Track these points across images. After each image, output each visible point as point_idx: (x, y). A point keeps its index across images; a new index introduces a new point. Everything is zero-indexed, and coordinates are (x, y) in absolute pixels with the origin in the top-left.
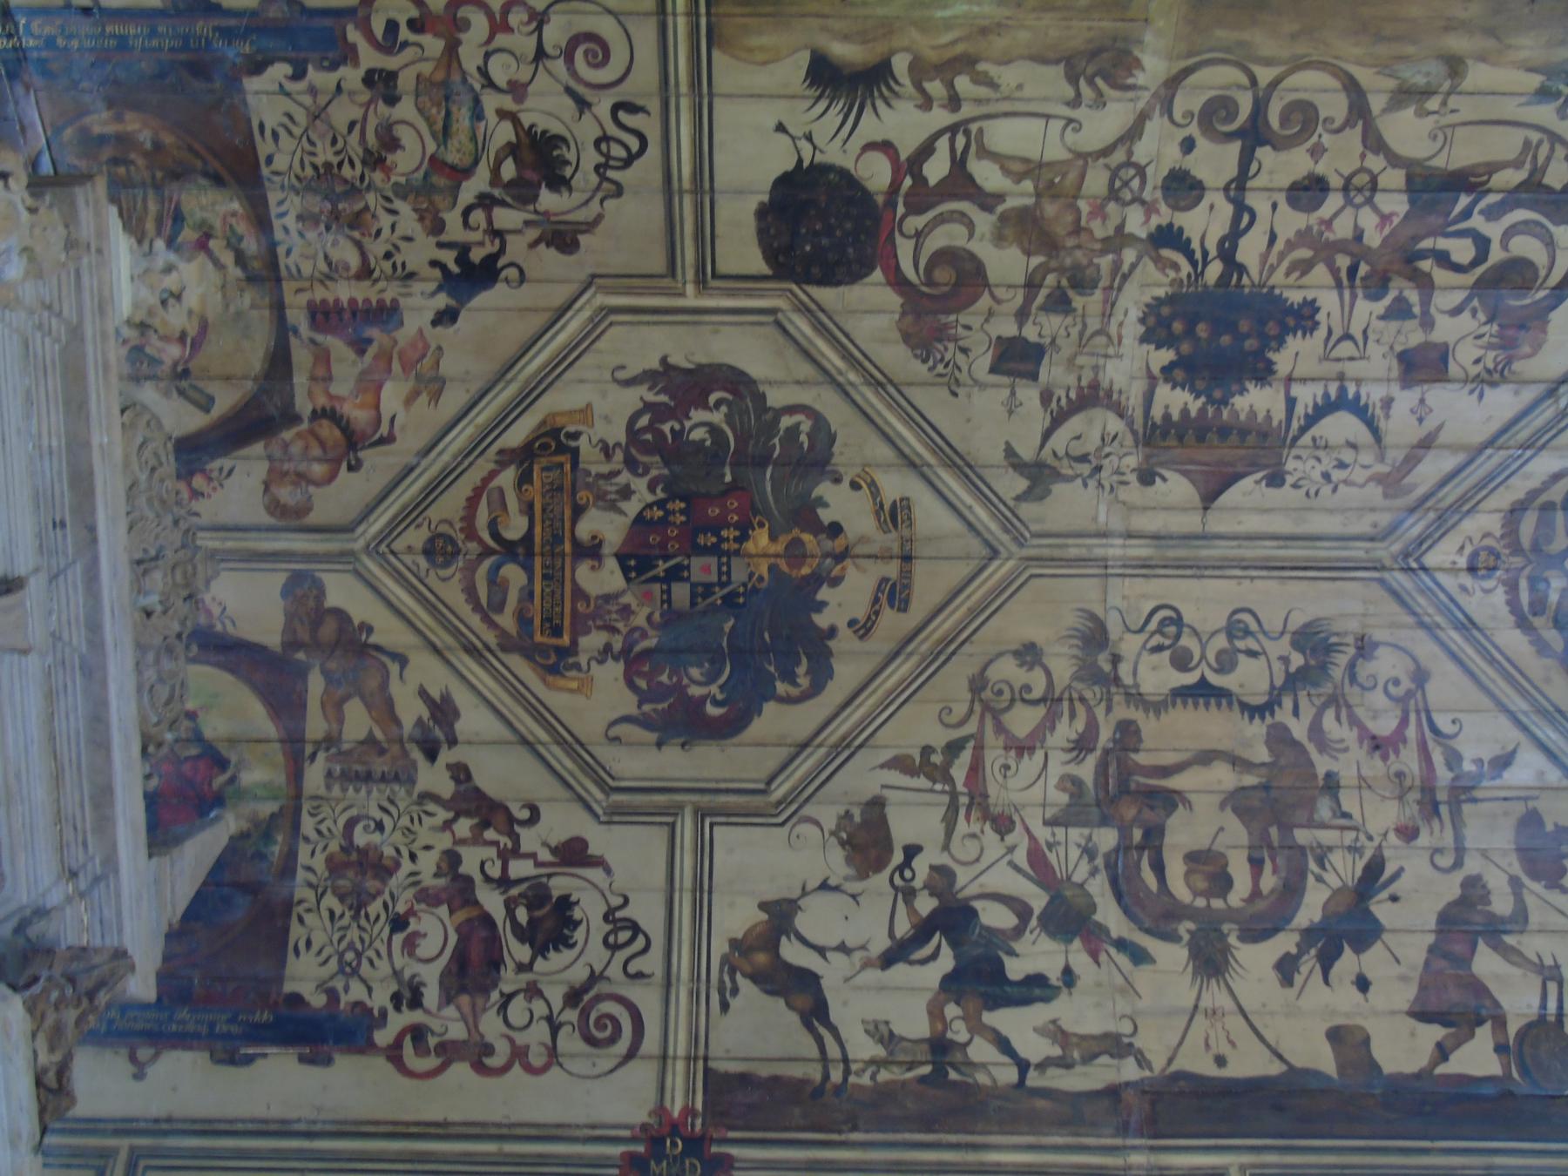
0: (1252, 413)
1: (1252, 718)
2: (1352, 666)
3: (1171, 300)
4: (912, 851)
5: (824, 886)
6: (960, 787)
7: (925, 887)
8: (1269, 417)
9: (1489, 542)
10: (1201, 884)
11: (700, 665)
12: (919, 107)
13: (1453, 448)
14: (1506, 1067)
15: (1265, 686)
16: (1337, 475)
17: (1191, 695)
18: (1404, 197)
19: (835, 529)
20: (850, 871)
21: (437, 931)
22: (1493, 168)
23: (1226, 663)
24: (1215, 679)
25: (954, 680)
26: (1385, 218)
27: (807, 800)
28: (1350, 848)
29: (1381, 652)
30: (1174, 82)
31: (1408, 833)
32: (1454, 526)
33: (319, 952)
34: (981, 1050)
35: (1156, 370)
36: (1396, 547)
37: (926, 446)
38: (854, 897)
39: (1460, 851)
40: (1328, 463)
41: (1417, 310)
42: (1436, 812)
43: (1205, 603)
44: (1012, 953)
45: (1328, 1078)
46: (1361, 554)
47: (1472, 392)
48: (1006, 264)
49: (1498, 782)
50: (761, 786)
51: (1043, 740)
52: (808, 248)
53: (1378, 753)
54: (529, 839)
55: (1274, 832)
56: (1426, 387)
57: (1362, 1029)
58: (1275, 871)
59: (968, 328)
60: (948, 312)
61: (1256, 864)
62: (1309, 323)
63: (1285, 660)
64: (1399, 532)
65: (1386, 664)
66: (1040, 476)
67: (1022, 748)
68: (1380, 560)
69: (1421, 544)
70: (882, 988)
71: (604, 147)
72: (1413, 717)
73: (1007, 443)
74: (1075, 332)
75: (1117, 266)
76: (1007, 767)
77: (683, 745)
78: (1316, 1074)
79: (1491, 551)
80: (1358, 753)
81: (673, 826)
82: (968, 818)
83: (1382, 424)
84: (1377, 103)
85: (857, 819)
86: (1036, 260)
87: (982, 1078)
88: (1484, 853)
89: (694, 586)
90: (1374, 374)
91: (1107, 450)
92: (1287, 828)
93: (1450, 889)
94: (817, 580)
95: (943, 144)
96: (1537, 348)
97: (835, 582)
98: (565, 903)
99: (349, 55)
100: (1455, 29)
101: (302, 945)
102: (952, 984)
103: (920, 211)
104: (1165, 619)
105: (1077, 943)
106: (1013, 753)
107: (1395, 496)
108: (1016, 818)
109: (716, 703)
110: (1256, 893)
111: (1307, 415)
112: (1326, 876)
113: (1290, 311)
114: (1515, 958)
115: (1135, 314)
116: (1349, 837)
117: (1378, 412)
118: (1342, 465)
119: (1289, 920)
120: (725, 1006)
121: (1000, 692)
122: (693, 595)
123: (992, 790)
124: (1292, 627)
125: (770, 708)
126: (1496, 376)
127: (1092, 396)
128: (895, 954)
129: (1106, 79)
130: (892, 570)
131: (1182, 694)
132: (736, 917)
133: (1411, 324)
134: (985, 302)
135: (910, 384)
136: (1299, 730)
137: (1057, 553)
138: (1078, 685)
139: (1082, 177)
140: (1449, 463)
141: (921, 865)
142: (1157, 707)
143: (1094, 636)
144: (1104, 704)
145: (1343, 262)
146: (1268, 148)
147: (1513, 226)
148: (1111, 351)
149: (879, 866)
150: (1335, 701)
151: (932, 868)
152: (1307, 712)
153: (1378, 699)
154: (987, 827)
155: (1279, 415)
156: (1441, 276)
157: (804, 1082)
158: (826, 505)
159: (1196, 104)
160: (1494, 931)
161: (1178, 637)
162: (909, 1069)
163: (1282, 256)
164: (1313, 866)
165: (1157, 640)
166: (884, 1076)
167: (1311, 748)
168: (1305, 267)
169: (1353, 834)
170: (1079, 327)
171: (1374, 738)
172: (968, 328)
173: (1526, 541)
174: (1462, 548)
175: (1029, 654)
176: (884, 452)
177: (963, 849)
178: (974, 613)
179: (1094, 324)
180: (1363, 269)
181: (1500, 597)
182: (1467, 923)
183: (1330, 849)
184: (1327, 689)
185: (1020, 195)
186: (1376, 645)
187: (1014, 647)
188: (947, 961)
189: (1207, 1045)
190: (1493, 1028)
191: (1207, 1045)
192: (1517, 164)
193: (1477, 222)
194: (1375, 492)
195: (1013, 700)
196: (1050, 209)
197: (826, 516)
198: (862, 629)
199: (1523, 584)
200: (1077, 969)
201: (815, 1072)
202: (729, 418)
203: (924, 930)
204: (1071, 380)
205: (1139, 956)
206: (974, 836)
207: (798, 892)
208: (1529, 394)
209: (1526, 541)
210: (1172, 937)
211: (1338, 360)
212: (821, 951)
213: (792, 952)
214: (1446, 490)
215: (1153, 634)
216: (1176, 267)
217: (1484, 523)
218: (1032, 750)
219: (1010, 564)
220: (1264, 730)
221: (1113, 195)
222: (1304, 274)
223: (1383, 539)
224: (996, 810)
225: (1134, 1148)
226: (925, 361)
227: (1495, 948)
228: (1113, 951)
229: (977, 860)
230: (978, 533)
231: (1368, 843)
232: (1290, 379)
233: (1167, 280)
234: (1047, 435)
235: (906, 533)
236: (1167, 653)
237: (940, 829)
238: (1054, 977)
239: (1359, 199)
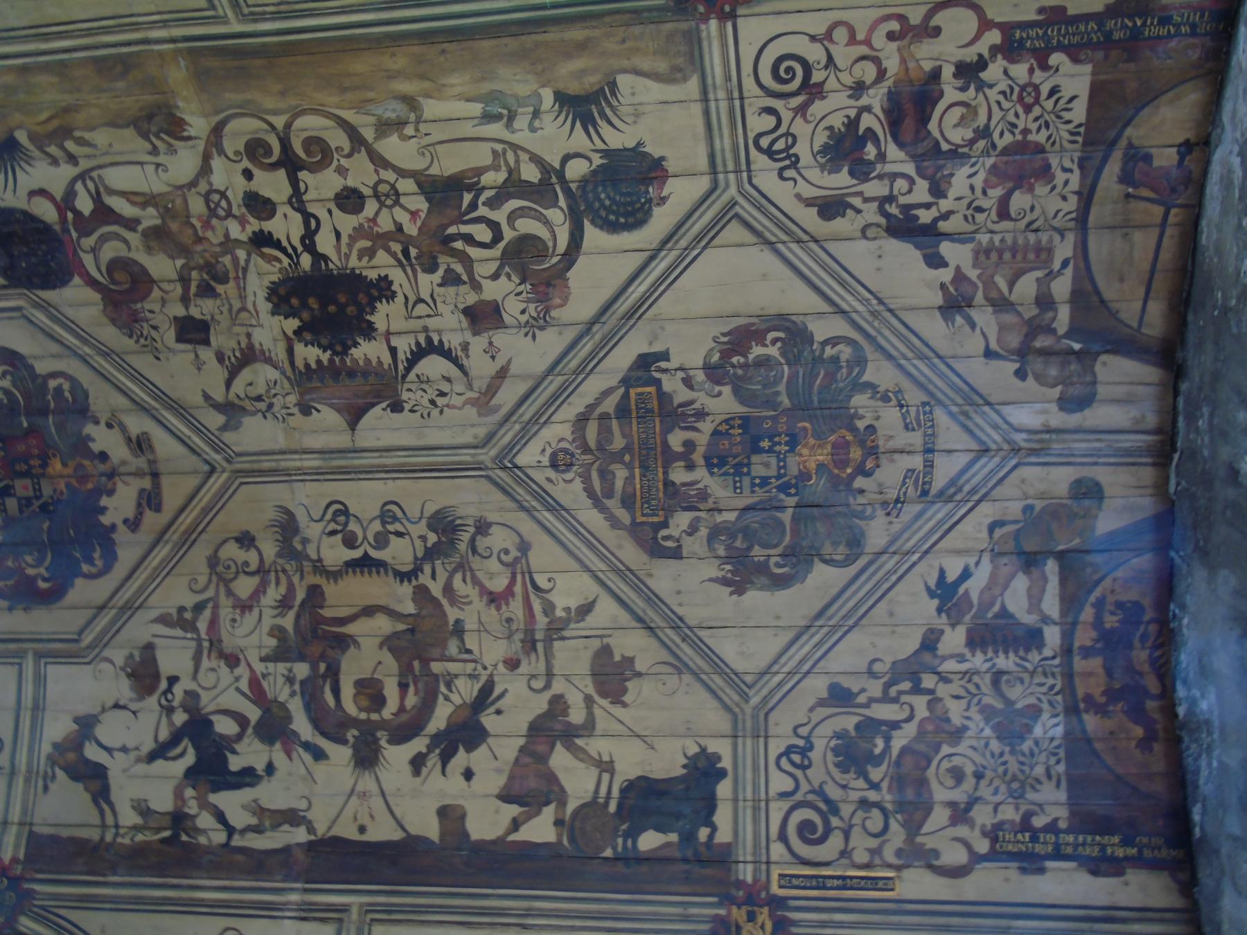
0: (368, 361)
1: (402, 581)
2: (473, 541)
3: (282, 282)
4: (173, 680)
5: (117, 706)
6: (203, 636)
7: (181, 706)
8: (380, 363)
9: (564, 445)
10: (365, 703)
11: (31, 554)
12: (50, 164)
13: (522, 377)
14: (559, 836)
15: (410, 558)
16: (440, 401)
17: (359, 566)
18: (422, 198)
19: (103, 456)
20: (133, 695)
22: (479, 171)
23: (381, 541)
24: (374, 554)
25: (198, 557)
26: (414, 214)
27: (105, 646)
28: (470, 676)
29: (494, 529)
30: (217, 130)
31: (512, 664)
32: (536, 433)
34: (205, 820)
35: (290, 334)
36: (493, 453)
37: (149, 395)
38: (134, 713)
39: (550, 675)
40: (432, 393)
41: (465, 277)
42: (534, 649)
43: (365, 498)
44: (234, 752)
45: (433, 842)
46: (468, 458)
47: (526, 335)
48: (161, 266)
49: (582, 625)
50: (75, 637)
51: (258, 602)
52: (24, 265)
53: (493, 605)
54: (871, 214)
55: (416, 664)
56: (491, 333)
57: (462, 807)
58: (416, 693)
59: (151, 312)
60: (136, 302)
61: (403, 687)
62: (389, 293)
63: (423, 538)
64: (493, 441)
65: (498, 539)
66: (232, 411)
67: (244, 607)
68: (482, 463)
69: (511, 449)
70: (147, 776)
72: (519, 578)
73: (203, 391)
74: (225, 309)
75: (235, 260)
76: (234, 620)
77: (25, 610)
78: (425, 840)
79: (565, 451)
80: (478, 604)
81: (20, 665)
82: (209, 657)
83: (465, 362)
84: (368, 134)
85: (137, 659)
86: (180, 262)
87: (202, 840)
88: (567, 678)
89: (19, 499)
90: (449, 325)
91: (273, 392)
92: (425, 662)
93: (540, 704)
94: (99, 492)
95: (79, 186)
96: (565, 300)
97: (111, 493)
100: (395, 77)
102: (192, 774)
103: (88, 234)
104: (336, 511)
105: (278, 746)
106: (238, 611)
107: (486, 415)
108: (241, 657)
109: (45, 580)
110: (402, 709)
111: (407, 359)
112: (452, 696)
113: (371, 284)
114: (582, 756)
115: (262, 294)
116: (470, 667)
117: (460, 353)
118: (442, 394)
119: (422, 729)
120: (46, 788)
121: (229, 567)
122: (20, 505)
123: (225, 636)
124: (427, 513)
125: (79, 582)
126: (542, 322)
127: (249, 356)
128: (160, 752)
129: (169, 134)
130: (147, 483)
131: (353, 565)
132: (57, 728)
133: (464, 289)
134: (156, 293)
135: (127, 353)
136: (436, 589)
137: (256, 466)
138: (280, 561)
139: (186, 202)
140: (522, 388)
141: (178, 690)
142: (334, 575)
143: (287, 526)
144: (298, 574)
145: (397, 247)
146: (305, 172)
147: (513, 212)
148: (254, 322)
149: (150, 690)
150: (461, 567)
151: (186, 692)
152: (442, 576)
153: (493, 564)
154: (222, 663)
155: (387, 359)
156: (474, 252)
157: (87, 841)
158: (93, 440)
159: (240, 145)
160: (569, 735)
161: (346, 524)
162: (157, 833)
163: (350, 246)
164: (443, 689)
165: (332, 526)
166: (140, 837)
167: (444, 602)
168: (370, 253)
169: (472, 665)
170: (227, 306)
171: (491, 593)
172: (151, 312)
173: (592, 443)
174: (544, 450)
175: (246, 540)
176: (122, 401)
177: (206, 679)
178: (205, 511)
179: (237, 305)
180: (413, 252)
181: (578, 485)
182: (553, 730)
183: (456, 676)
184: (456, 559)
185: (150, 218)
186: (490, 525)
187: (234, 535)
188: (190, 759)
189: (355, 819)
190: (557, 808)
191: (355, 819)
192: (496, 168)
193: (482, 211)
194: (471, 412)
195: (237, 573)
196: (174, 226)
197: (96, 447)
198: (134, 524)
199: (595, 475)
200: (276, 764)
201: (94, 835)
202: (14, 384)
203: (175, 739)
204: (233, 344)
205: (319, 755)
206: (213, 670)
207: (99, 709)
208: (570, 334)
209: (592, 443)
210: (343, 742)
211: (420, 317)
212: (108, 750)
213: (92, 752)
214: (523, 408)
215: (329, 522)
216: (279, 261)
217: (558, 431)
218: (250, 608)
219: (225, 475)
220: (411, 590)
221: (212, 212)
222: (371, 258)
223: (483, 446)
224: (228, 651)
225: (292, 889)
226: (131, 337)
227: (568, 749)
228: (301, 750)
229: (215, 687)
230: (199, 455)
231: (483, 672)
232: (388, 334)
233: (276, 270)
234: (228, 384)
235: (151, 457)
236: (340, 536)
237: (190, 665)
238: (260, 767)
239: (389, 202)
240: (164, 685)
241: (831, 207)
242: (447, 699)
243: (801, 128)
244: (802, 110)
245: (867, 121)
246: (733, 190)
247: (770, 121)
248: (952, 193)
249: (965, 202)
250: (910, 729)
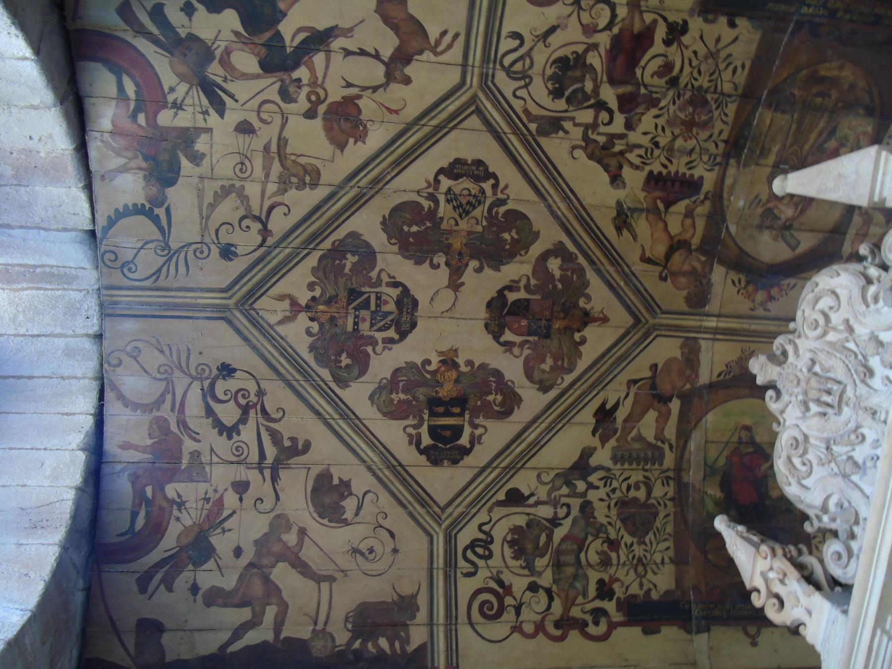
21: (648, 68)
33: (729, 64)
54: (577, 133)
71: (487, 553)
98: (556, 94)
99: (620, 606)
101: (739, 70)
141: (303, 104)
240: (322, 109)
242: (178, 519)
248: (641, 128)
249: (649, 137)
250: (567, 524)
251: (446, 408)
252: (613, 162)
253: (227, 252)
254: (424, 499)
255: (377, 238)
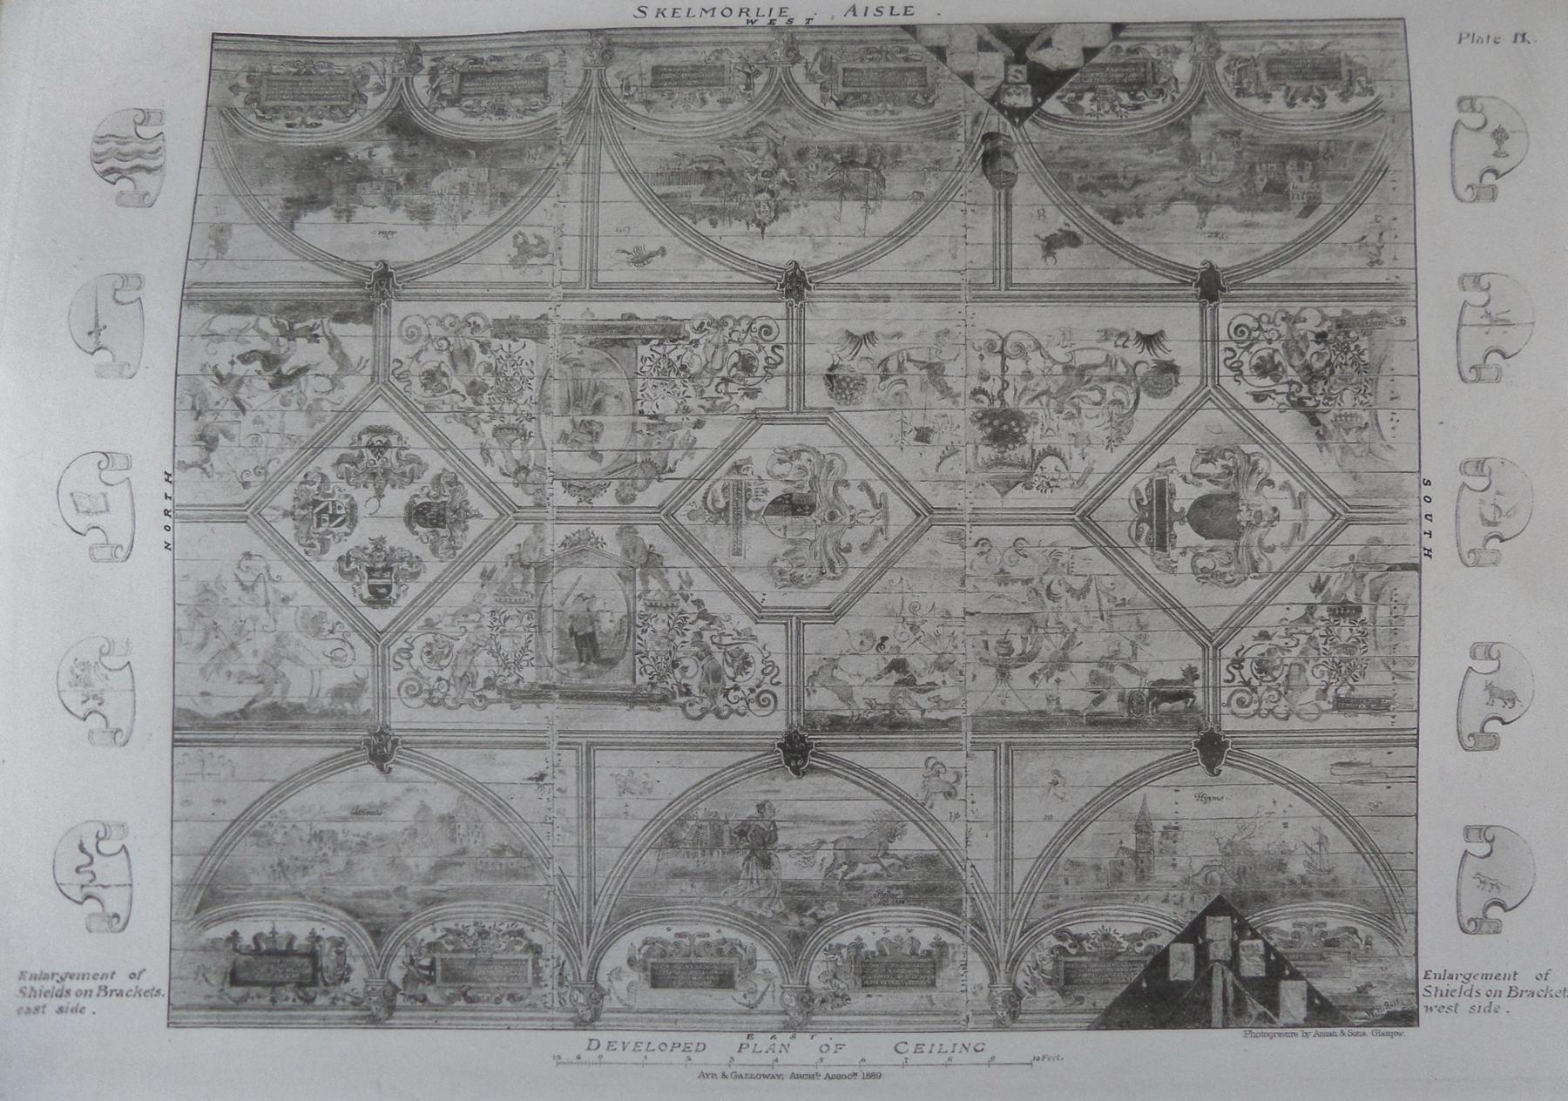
238: (939, 682)
241: (1258, 397)
243: (1245, 358)
244: (1247, 348)
245: (1277, 358)
246: (1210, 387)
247: (1230, 354)
251: (381, 575)
252: (472, 422)
253: (245, 485)
254: (368, 625)
255: (332, 475)
